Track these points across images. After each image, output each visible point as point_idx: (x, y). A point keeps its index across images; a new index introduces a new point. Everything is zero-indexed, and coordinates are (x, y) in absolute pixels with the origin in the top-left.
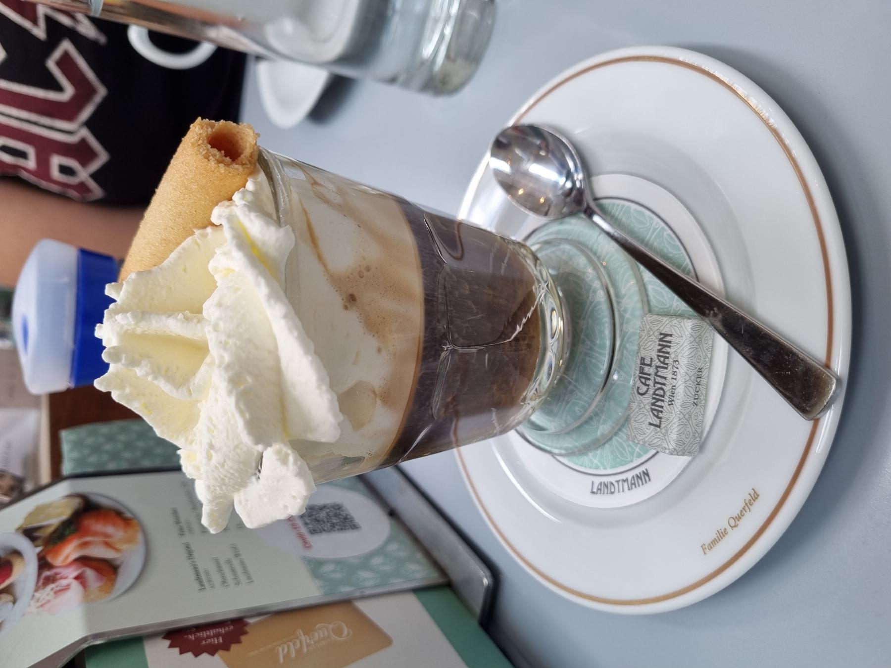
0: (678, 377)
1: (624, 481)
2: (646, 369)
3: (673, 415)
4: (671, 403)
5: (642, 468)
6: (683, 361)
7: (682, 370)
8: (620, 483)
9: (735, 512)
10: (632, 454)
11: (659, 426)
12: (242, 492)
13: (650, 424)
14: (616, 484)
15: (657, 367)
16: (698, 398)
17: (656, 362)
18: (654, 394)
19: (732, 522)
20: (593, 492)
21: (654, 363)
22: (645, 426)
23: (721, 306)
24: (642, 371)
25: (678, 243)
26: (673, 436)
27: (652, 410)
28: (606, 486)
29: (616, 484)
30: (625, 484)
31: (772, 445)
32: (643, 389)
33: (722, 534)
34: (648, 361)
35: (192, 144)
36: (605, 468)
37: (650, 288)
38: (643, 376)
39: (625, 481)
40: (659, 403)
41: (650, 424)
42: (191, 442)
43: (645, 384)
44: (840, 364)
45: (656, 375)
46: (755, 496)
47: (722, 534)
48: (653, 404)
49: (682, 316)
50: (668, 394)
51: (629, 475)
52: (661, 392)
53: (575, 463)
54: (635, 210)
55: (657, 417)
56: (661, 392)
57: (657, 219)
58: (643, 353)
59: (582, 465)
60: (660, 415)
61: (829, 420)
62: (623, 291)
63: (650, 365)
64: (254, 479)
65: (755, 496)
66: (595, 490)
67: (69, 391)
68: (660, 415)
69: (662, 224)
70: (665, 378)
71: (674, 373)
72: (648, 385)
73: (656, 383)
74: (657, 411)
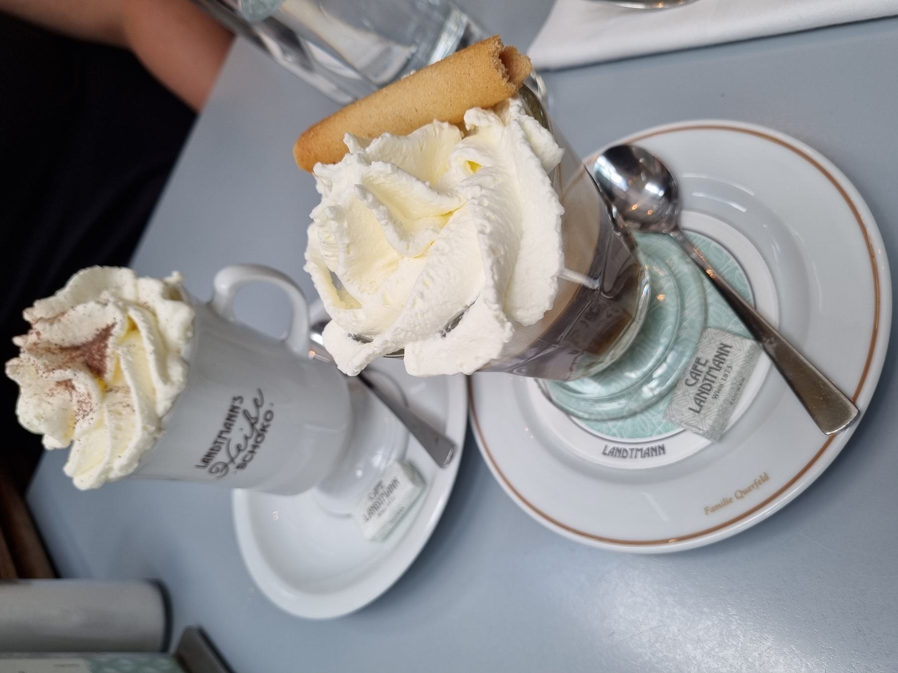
0: (728, 379)
1: (638, 450)
2: (700, 367)
3: (713, 407)
4: (715, 397)
5: (660, 444)
6: (736, 368)
7: (733, 375)
8: (634, 452)
9: (744, 486)
10: (653, 431)
11: (698, 412)
12: (418, 344)
13: (691, 409)
14: (630, 452)
15: (711, 368)
16: (733, 401)
17: (711, 364)
18: (701, 387)
19: (739, 494)
20: (604, 453)
21: (708, 365)
22: (685, 409)
23: (776, 338)
24: (695, 368)
25: (746, 282)
26: (709, 422)
27: (696, 399)
28: (619, 451)
29: (630, 452)
30: (639, 454)
31: (800, 444)
32: (693, 381)
33: (726, 502)
34: (703, 361)
35: (489, 53)
36: (622, 437)
37: (711, 309)
38: (695, 372)
39: (641, 450)
40: (704, 395)
41: (691, 409)
42: (362, 292)
43: (695, 378)
44: (863, 402)
45: (708, 373)
46: (765, 478)
47: (726, 502)
48: (698, 395)
49: (745, 337)
50: (715, 389)
51: (645, 447)
52: (709, 387)
53: (592, 428)
54: (715, 248)
55: (699, 405)
56: (709, 387)
57: (732, 259)
58: (699, 355)
59: (599, 431)
60: (702, 404)
61: (843, 436)
62: (687, 305)
63: (704, 365)
64: (439, 335)
65: (765, 478)
66: (607, 452)
67: (311, 212)
68: (702, 404)
69: (737, 264)
70: (715, 377)
71: (726, 375)
72: (697, 380)
73: (705, 379)
74: (700, 399)
